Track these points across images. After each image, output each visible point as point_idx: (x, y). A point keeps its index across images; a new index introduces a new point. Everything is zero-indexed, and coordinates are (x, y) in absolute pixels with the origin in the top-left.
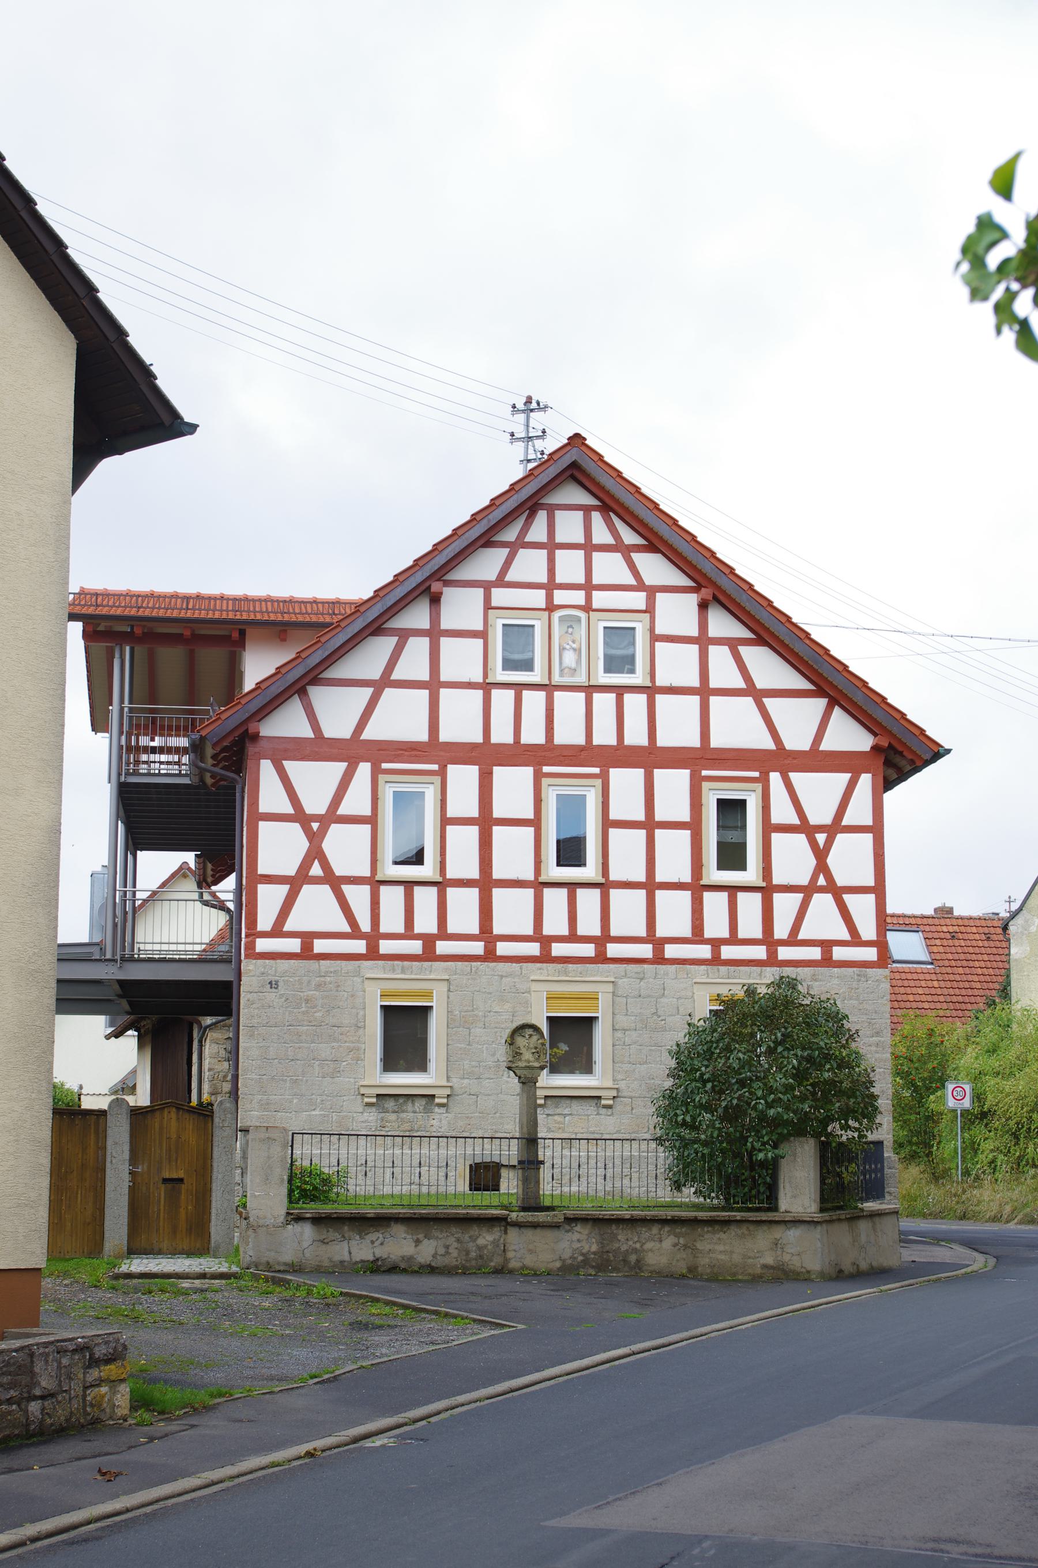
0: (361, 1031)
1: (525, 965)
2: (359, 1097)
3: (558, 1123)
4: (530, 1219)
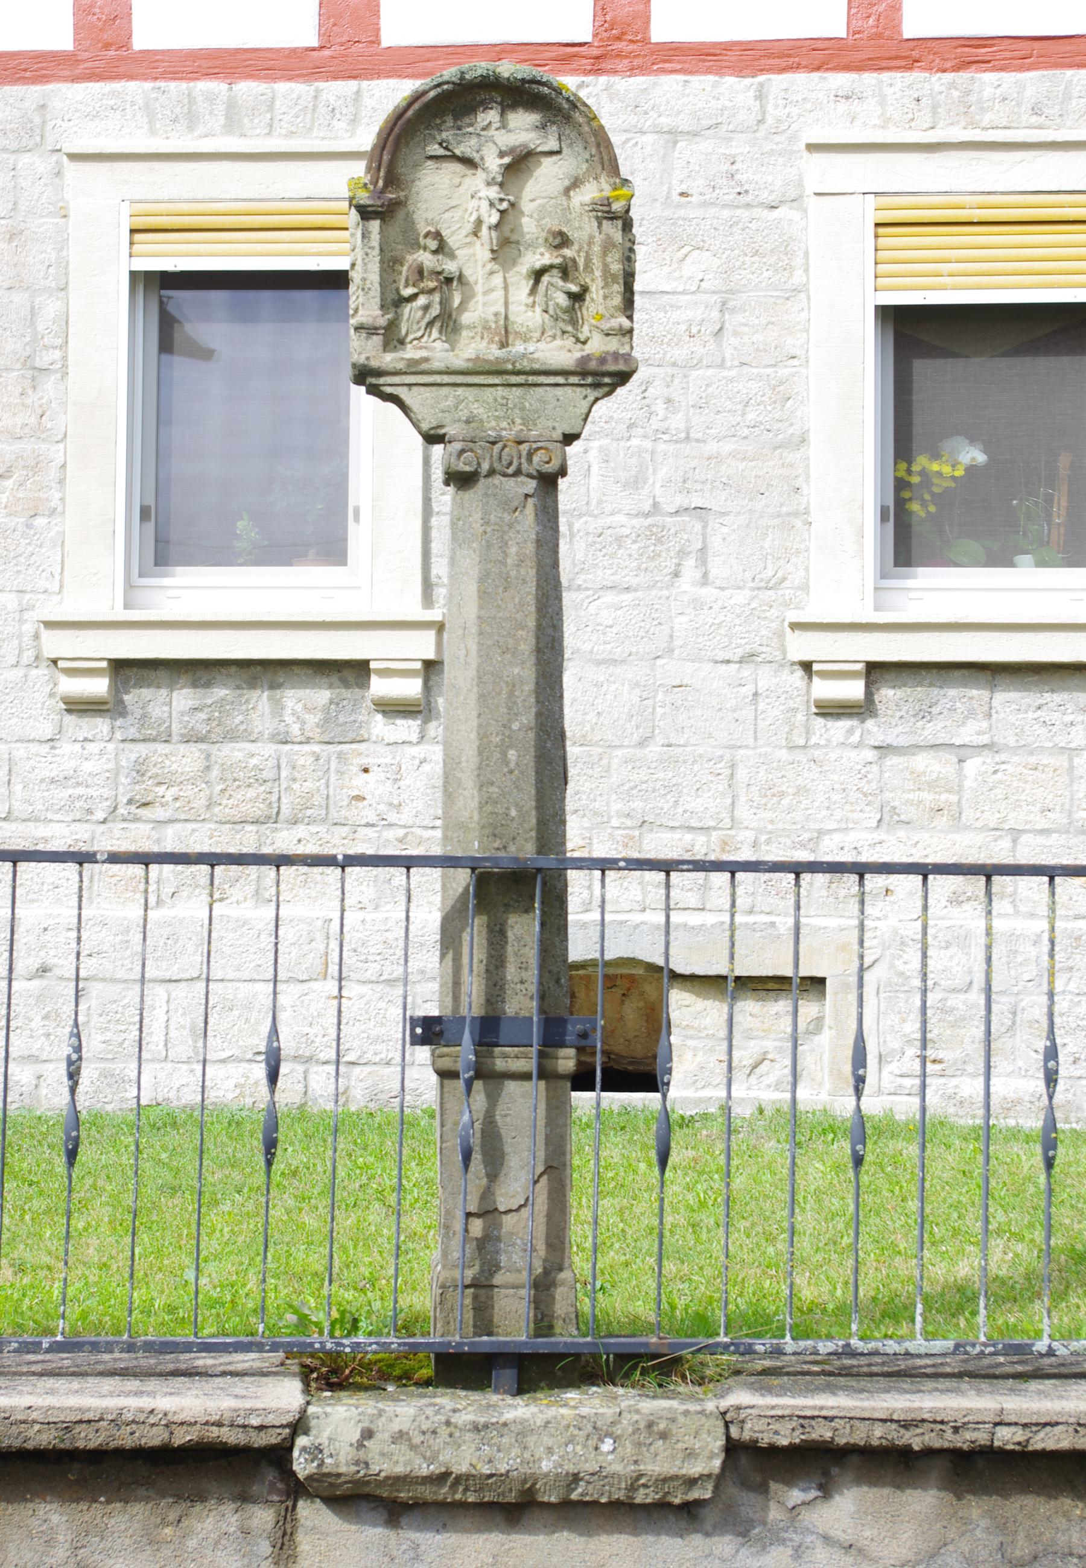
0: (50, 385)
1: (777, 82)
2: (42, 673)
3: (932, 785)
4: (465, 1458)
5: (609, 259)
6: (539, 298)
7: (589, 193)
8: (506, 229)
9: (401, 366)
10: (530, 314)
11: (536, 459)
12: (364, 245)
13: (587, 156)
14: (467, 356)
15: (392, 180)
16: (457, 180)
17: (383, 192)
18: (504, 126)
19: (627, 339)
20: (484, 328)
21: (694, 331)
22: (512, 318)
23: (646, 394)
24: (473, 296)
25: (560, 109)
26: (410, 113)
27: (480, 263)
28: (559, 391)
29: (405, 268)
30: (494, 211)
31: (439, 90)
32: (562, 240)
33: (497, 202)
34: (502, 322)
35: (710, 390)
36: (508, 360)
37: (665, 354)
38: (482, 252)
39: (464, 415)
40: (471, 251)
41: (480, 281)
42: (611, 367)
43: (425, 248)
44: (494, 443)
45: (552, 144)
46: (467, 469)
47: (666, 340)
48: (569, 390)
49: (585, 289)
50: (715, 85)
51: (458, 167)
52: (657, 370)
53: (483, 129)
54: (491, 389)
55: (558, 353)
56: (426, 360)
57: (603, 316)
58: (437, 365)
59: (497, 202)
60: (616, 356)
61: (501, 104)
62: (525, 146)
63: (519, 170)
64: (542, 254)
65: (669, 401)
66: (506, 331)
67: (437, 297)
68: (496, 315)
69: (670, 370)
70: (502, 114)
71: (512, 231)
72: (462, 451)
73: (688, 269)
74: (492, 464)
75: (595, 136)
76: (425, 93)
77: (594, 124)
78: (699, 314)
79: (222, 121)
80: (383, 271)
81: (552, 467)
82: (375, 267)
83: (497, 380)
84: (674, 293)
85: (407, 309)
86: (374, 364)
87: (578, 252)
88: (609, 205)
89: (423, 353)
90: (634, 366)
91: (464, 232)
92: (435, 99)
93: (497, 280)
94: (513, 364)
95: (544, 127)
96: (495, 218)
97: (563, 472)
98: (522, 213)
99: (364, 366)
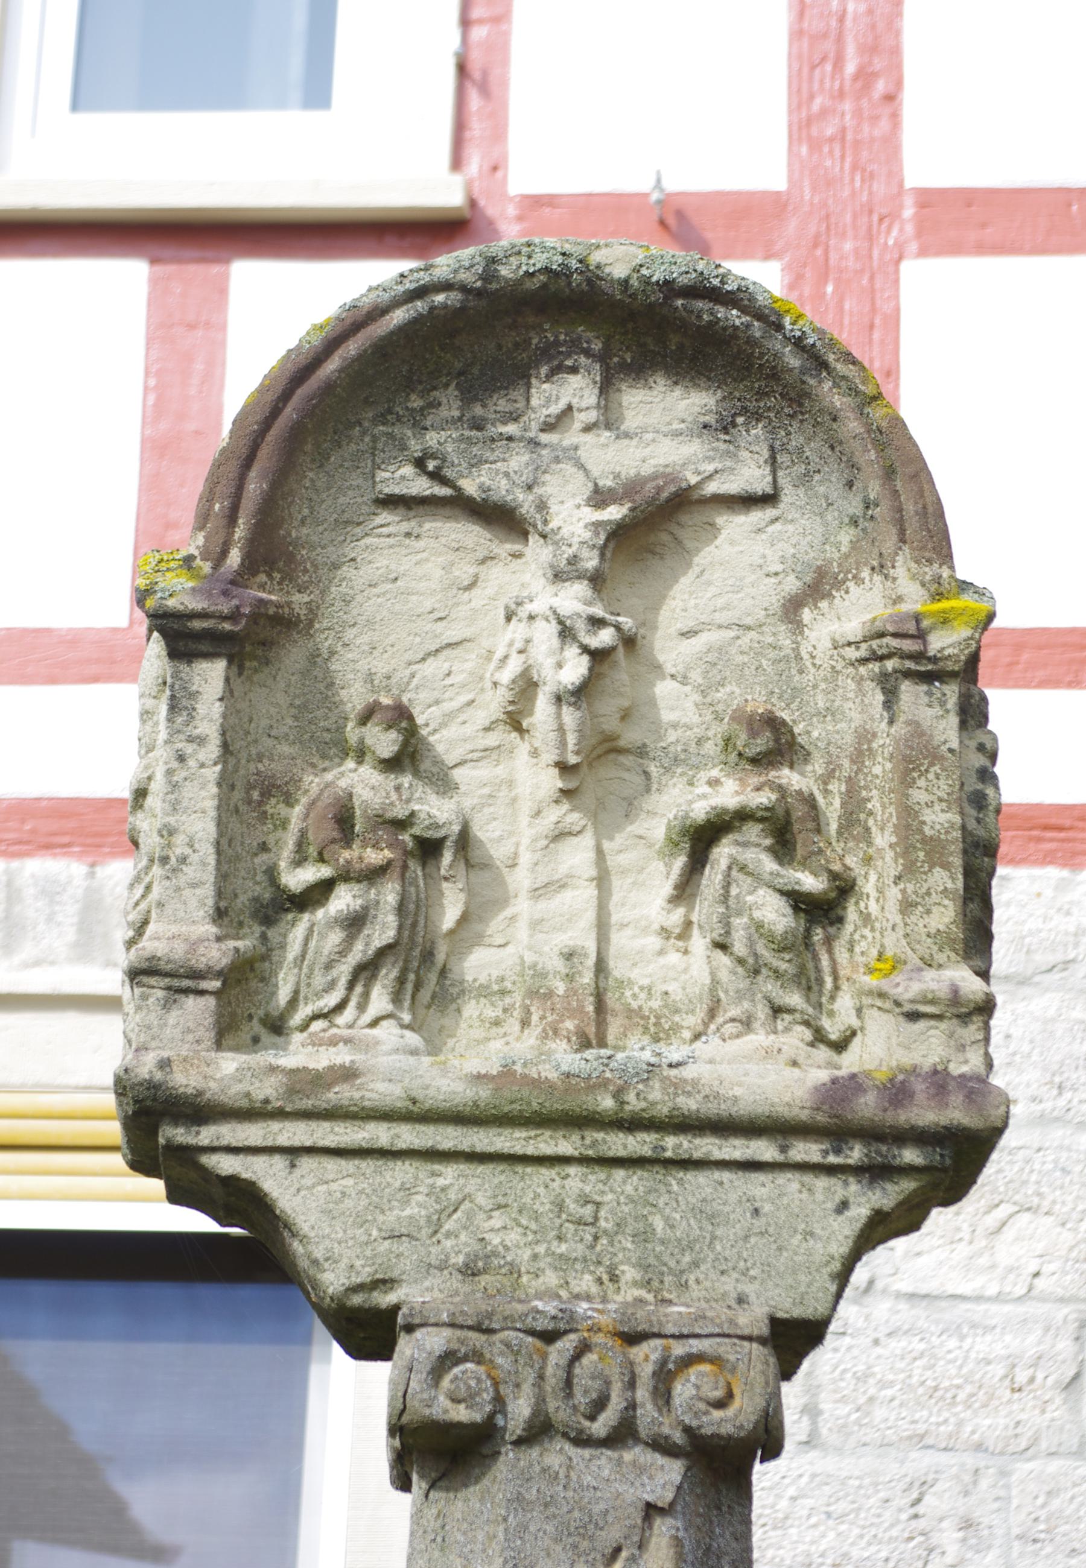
5: (918, 796)
6: (705, 907)
7: (857, 610)
8: (608, 708)
9: (267, 1089)
10: (674, 958)
11: (683, 1391)
12: (173, 733)
13: (854, 506)
14: (474, 1065)
15: (271, 550)
16: (464, 571)
17: (238, 580)
18: (608, 420)
19: (972, 1032)
20: (532, 993)
21: (1022, 1377)
22: (618, 968)
23: (920, 1509)
24: (503, 901)
25: (774, 373)
26: (332, 365)
27: (526, 808)
28: (759, 1186)
29: (298, 810)
30: (572, 652)
31: (420, 306)
32: (772, 743)
33: (581, 626)
34: (587, 978)
35: (1056, 1504)
36: (604, 1084)
37: (960, 1424)
38: (531, 774)
39: (458, 1247)
40: (501, 771)
41: (525, 859)
42: (925, 1114)
43: (361, 754)
44: (549, 1337)
45: (751, 475)
46: (462, 1414)
47: (962, 1396)
48: (790, 1182)
49: (844, 888)
50: (1061, 886)
51: (471, 534)
52: (944, 1458)
53: (548, 427)
54: (546, 1173)
55: (761, 1068)
56: (348, 1074)
57: (898, 963)
58: (380, 1090)
59: (581, 626)
60: (940, 1081)
61: (602, 358)
62: (671, 478)
63: (651, 551)
64: (714, 783)
65: (967, 1524)
66: (600, 1006)
67: (389, 893)
68: (569, 956)
69: (971, 1460)
70: (606, 387)
71: (626, 715)
72: (447, 1360)
73: (1006, 1251)
74: (540, 1400)
75: (881, 447)
76: (378, 312)
77: (877, 413)
78: (1030, 1343)
79: (71, 935)
80: (226, 812)
81: (735, 1419)
82: (203, 795)
83: (565, 1146)
84: (979, 1299)
85: (297, 931)
86: (185, 1080)
87: (825, 780)
88: (921, 635)
89: (341, 1056)
90: (995, 1115)
91: (481, 716)
92: (406, 331)
93: (577, 856)
94: (618, 1095)
95: (726, 427)
96: (574, 669)
97: (767, 1440)
98: (657, 668)
99: (152, 1086)
